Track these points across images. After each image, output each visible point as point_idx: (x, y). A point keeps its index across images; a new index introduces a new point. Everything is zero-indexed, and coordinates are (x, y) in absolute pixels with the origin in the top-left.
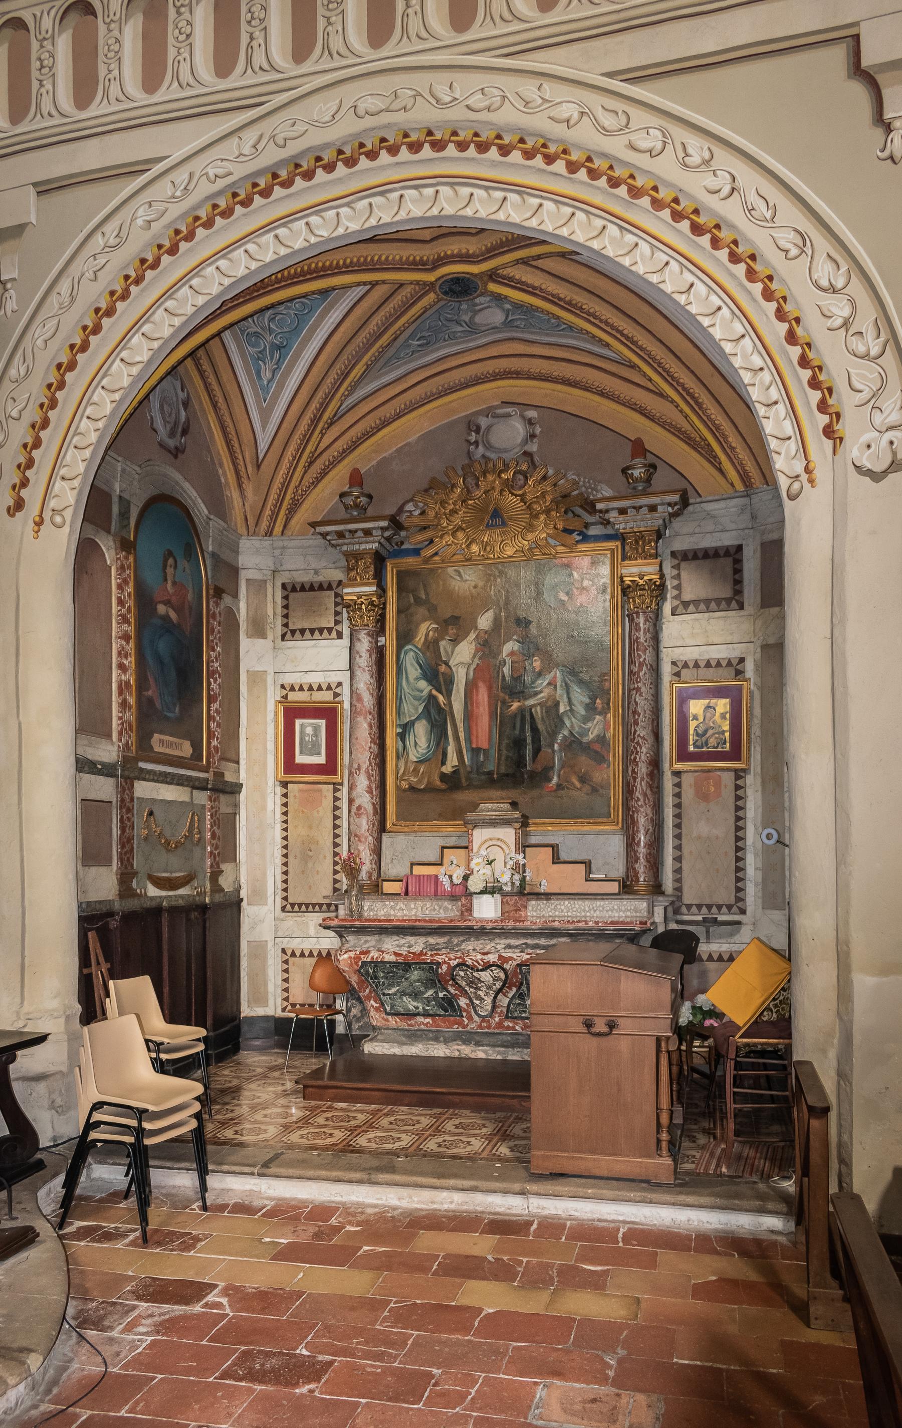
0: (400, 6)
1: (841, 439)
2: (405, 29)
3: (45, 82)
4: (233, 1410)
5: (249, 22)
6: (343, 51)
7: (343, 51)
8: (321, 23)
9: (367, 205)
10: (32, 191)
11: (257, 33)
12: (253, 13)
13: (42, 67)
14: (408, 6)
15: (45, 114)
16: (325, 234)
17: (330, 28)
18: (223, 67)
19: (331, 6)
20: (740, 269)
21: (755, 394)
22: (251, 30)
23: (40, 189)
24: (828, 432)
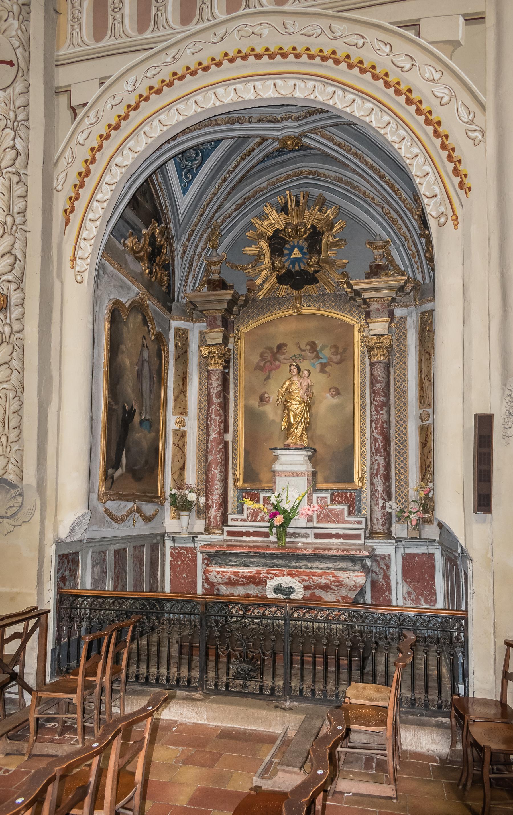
0: (199, 2)
1: (470, 189)
2: (156, 23)
3: (161, 8)
4: (312, 306)
5: (113, 10)
6: (80, 43)
7: (80, 43)
8: (154, 11)
9: (293, 84)
10: (461, 20)
11: (76, 26)
12: (74, 14)
13: (115, 8)
14: (203, 3)
15: (117, 36)
16: (283, 92)
17: (74, 32)
18: (142, 27)
19: (116, 10)
20: (430, 129)
21: (414, 171)
22: (72, 24)
23: (466, 18)
24: (461, 185)
